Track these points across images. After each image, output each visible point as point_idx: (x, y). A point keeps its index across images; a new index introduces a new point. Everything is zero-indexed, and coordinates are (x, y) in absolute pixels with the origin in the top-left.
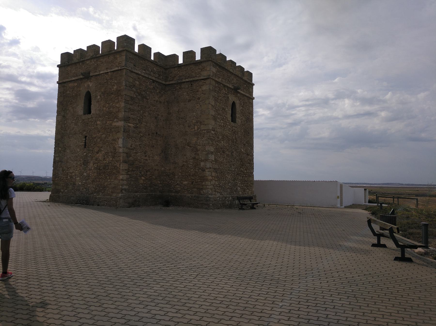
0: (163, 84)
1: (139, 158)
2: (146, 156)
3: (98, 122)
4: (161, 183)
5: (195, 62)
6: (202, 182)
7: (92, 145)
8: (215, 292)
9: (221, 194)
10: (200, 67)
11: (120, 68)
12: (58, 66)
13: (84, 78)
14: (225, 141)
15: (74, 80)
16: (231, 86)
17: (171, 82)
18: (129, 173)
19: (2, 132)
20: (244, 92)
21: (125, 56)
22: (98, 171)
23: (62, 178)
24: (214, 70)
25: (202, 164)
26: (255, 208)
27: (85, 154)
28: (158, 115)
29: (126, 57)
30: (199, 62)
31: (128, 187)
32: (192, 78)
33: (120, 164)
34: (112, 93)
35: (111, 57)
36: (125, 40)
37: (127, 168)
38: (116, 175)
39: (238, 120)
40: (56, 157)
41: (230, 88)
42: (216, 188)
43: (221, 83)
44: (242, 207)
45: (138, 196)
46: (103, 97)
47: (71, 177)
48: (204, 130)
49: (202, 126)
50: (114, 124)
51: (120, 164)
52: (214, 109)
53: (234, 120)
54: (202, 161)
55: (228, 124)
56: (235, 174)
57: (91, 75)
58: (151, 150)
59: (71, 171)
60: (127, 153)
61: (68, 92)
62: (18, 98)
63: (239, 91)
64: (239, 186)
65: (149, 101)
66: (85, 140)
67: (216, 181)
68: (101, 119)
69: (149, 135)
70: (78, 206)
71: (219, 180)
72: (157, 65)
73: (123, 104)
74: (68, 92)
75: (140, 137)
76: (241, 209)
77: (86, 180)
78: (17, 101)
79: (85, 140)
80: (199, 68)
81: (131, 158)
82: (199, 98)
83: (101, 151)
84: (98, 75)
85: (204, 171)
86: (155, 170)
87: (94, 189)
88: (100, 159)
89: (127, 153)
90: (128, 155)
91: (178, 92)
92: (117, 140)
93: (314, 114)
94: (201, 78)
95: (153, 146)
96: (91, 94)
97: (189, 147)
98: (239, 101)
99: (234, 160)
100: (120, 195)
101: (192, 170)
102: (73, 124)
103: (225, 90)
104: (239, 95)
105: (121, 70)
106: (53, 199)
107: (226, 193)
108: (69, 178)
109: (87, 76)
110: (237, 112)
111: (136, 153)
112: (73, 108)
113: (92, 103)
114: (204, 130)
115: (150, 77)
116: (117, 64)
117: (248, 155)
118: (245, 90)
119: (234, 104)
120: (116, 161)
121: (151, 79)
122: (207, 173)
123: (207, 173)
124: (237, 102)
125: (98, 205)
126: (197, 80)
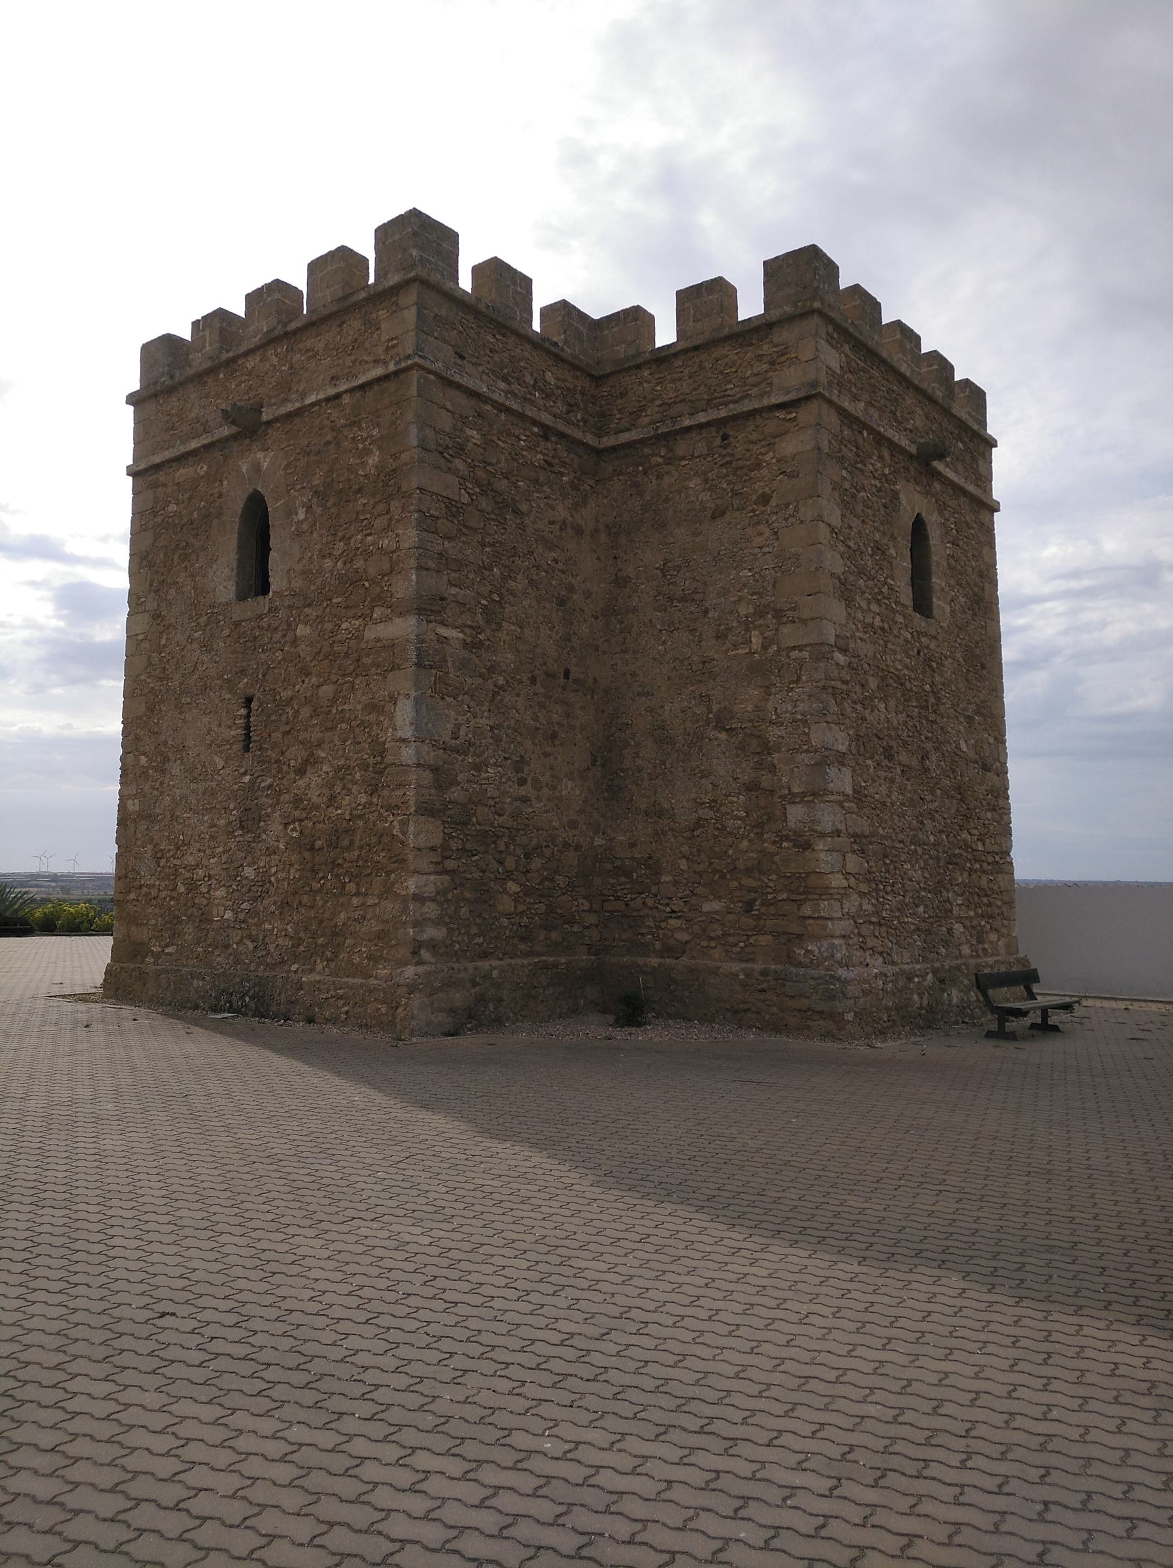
0: (586, 445)
1: (491, 791)
2: (522, 782)
3: (302, 630)
4: (591, 910)
5: (736, 329)
6: (800, 904)
7: (277, 736)
8: (689, 1229)
9: (888, 959)
10: (766, 348)
11: (392, 367)
12: (132, 399)
13: (235, 437)
14: (892, 703)
15: (193, 453)
16: (904, 443)
17: (625, 437)
18: (450, 864)
19: (15, 728)
20: (956, 472)
21: (414, 309)
22: (307, 855)
23: (154, 892)
24: (833, 359)
25: (796, 814)
26: (1055, 1029)
27: (247, 779)
28: (571, 589)
29: (419, 312)
30: (759, 328)
31: (445, 930)
32: (726, 404)
33: (404, 824)
34: (359, 491)
35: (354, 325)
36: (415, 234)
37: (437, 841)
38: (388, 873)
39: (940, 605)
40: (130, 797)
41: (903, 451)
42: (865, 929)
43: (865, 426)
44: (1002, 1027)
45: (495, 974)
46: (319, 510)
47: (192, 886)
48: (800, 648)
49: (786, 630)
50: (371, 633)
51: (404, 824)
52: (842, 548)
53: (922, 605)
54: (793, 798)
55: (900, 619)
56: (938, 859)
57: (265, 417)
58: (546, 755)
59: (190, 860)
60: (435, 770)
61: (173, 507)
62: (65, 612)
63: (938, 465)
64: (959, 920)
65: (527, 521)
66: (248, 716)
67: (862, 894)
68: (313, 613)
69: (533, 680)
70: (217, 1028)
71: (877, 890)
72: (559, 359)
73: (410, 536)
74: (173, 507)
75: (495, 694)
76: (1000, 1034)
77: (255, 899)
78: (61, 624)
79: (248, 716)
80: (759, 358)
81: (455, 794)
82: (765, 499)
83: (319, 761)
84: (298, 413)
85: (807, 846)
86: (566, 845)
87: (288, 943)
88: (315, 799)
89: (435, 770)
90: (441, 777)
91: (659, 477)
92: (390, 707)
93: (1104, 624)
94: (775, 400)
95: (554, 736)
96: (269, 504)
97: (723, 736)
98: (941, 514)
99: (932, 792)
100: (410, 972)
101: (745, 843)
102: (195, 646)
103: (881, 457)
104: (937, 486)
105: (396, 373)
106: (120, 986)
107: (907, 956)
108: (182, 889)
109: (249, 426)
110: (934, 568)
111: (477, 767)
112: (192, 576)
113: (273, 542)
114: (800, 648)
115: (530, 412)
116: (380, 350)
117: (986, 768)
118: (960, 467)
119: (919, 525)
120: (389, 808)
121: (535, 422)
122: (824, 857)
123: (824, 857)
124: (933, 520)
125: (310, 1020)
126: (752, 414)
